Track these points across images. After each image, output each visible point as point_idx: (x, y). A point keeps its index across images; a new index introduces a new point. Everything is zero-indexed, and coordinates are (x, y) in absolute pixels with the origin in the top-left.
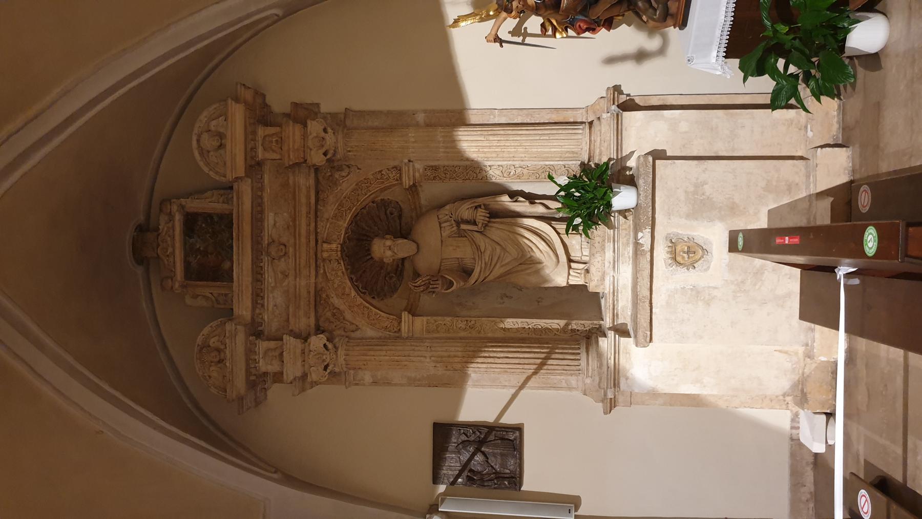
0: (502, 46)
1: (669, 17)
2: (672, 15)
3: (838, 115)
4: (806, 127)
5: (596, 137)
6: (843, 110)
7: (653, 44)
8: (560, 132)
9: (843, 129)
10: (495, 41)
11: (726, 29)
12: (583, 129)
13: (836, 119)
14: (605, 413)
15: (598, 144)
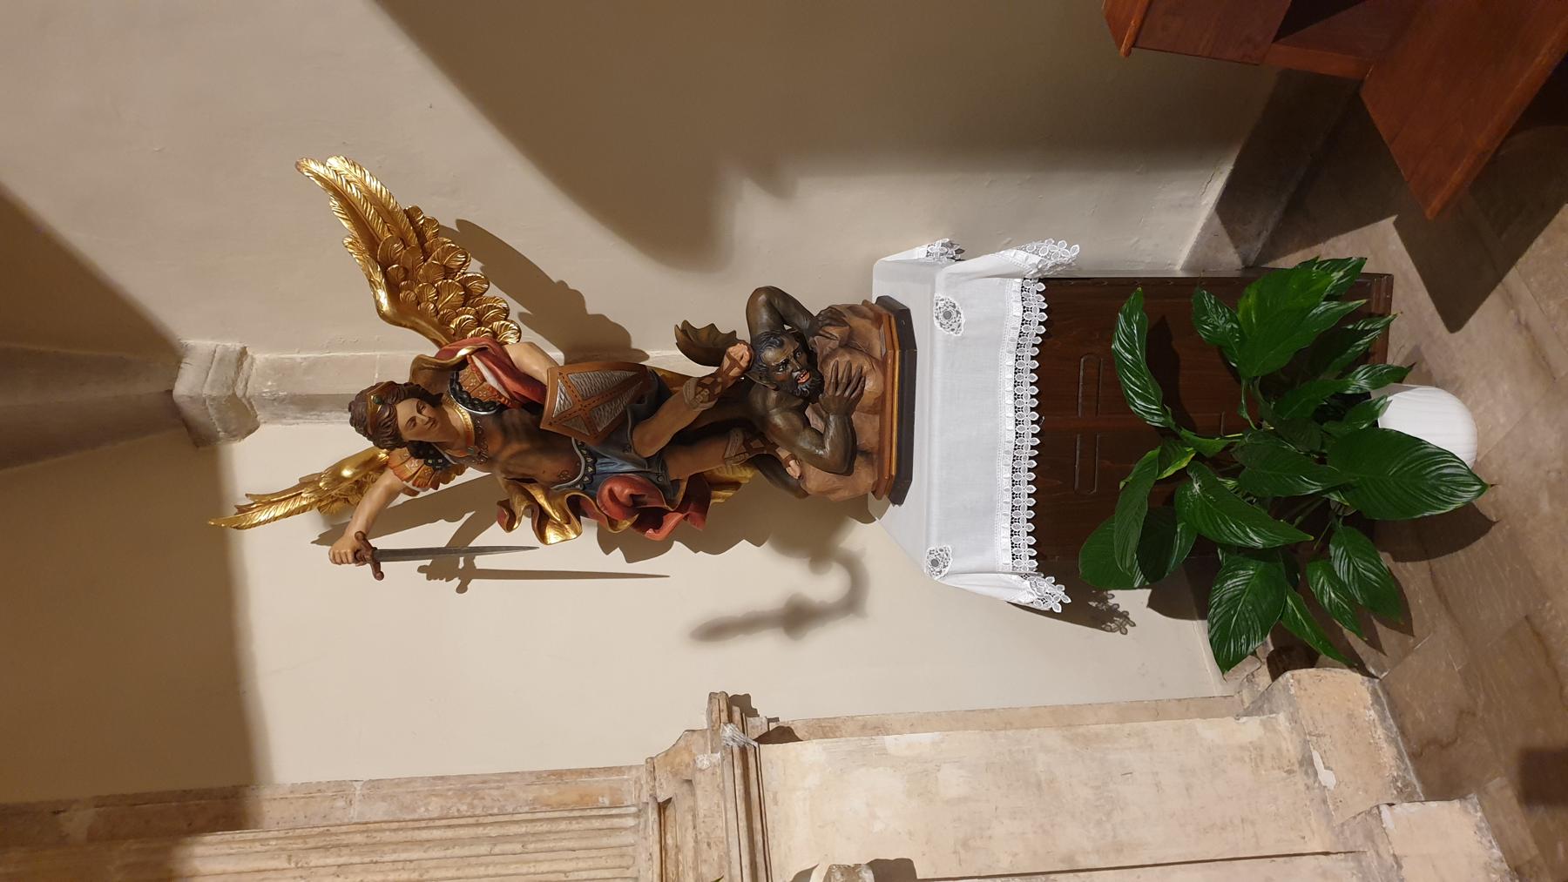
0: (379, 575)
1: (859, 460)
2: (866, 454)
3: (1383, 719)
4: (1307, 762)
5: (682, 834)
6: (1394, 705)
7: (827, 586)
8: (563, 826)
9: (1414, 757)
10: (358, 558)
11: (1029, 452)
12: (635, 829)
13: (1380, 732)
14: (686, 323)
15: (688, 854)
